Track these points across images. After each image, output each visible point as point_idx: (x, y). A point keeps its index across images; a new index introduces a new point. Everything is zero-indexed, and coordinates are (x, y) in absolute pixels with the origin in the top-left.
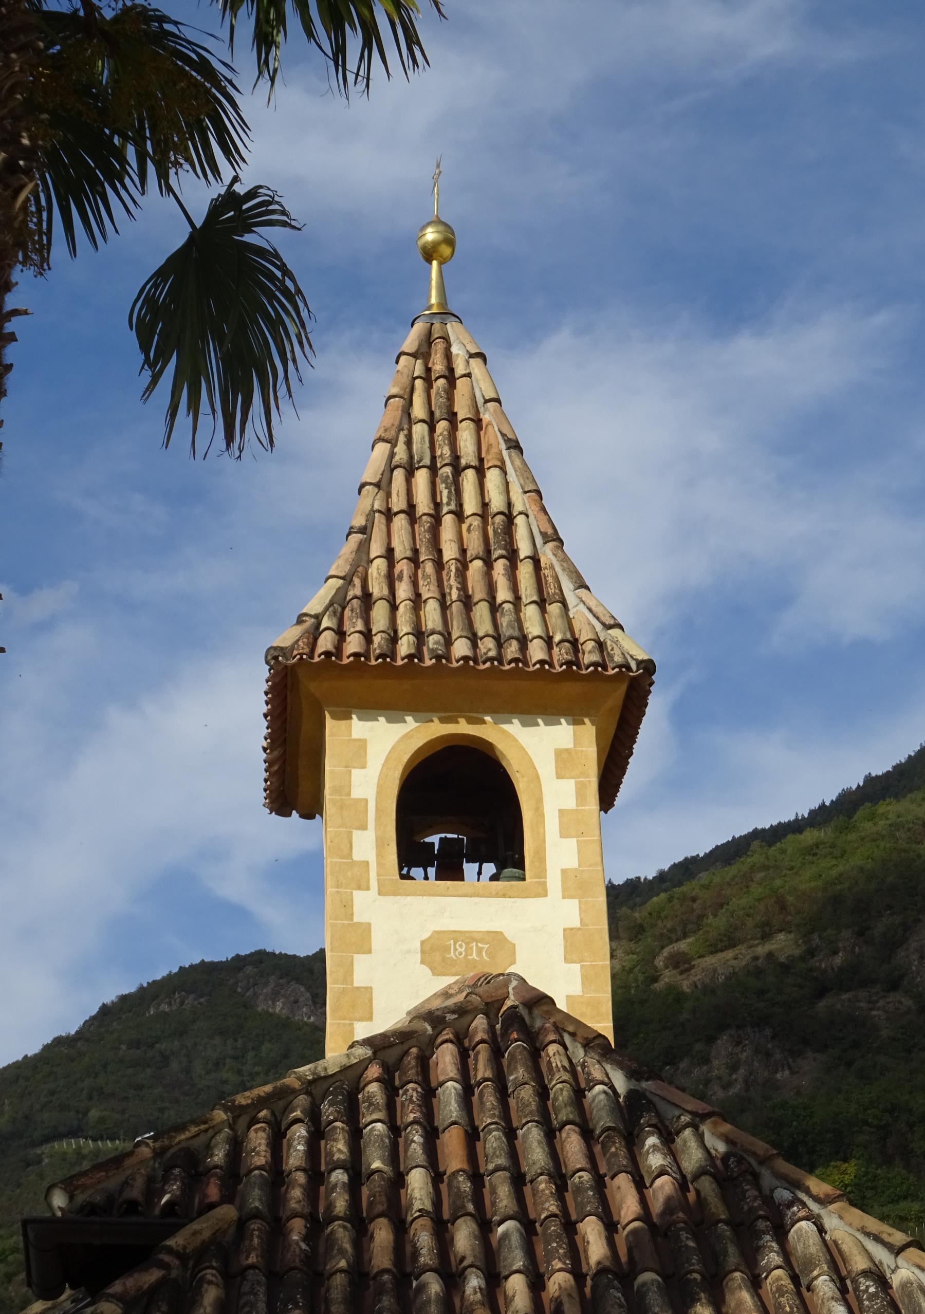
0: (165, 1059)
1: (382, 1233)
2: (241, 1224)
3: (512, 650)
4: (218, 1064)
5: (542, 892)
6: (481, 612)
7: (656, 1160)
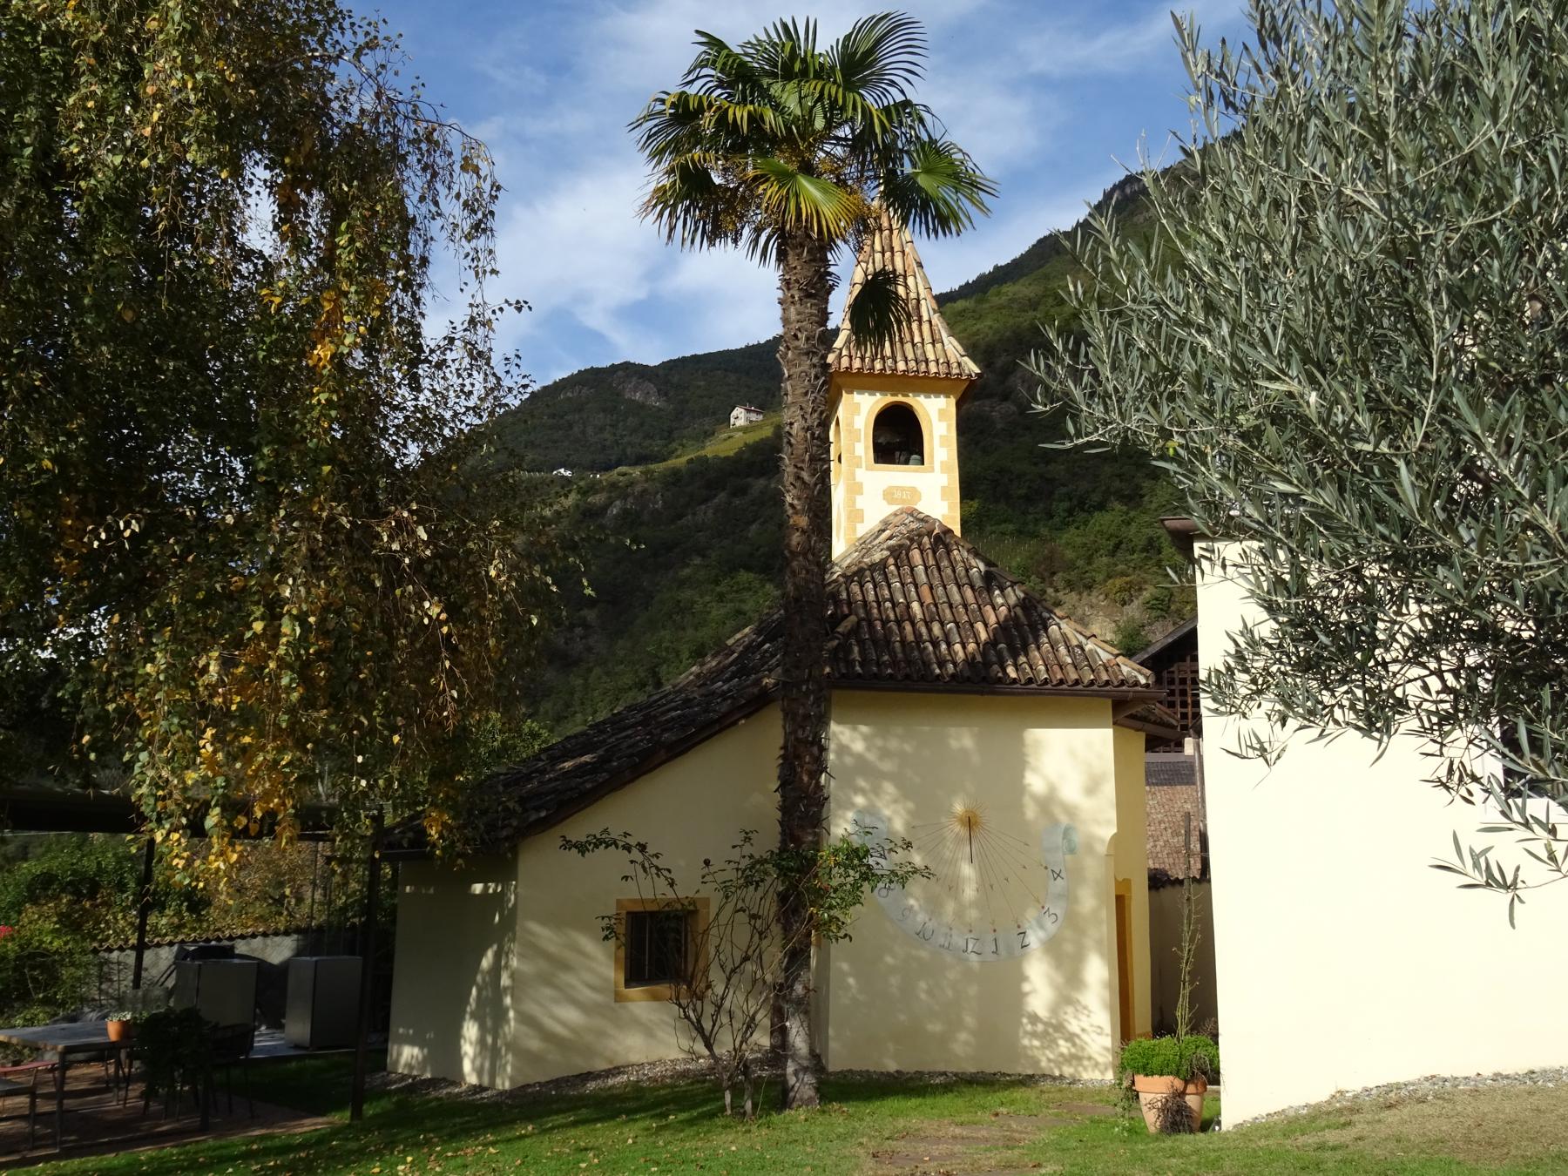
0: (571, 426)
1: (908, 627)
2: (858, 623)
3: (923, 367)
4: (602, 429)
5: (932, 470)
6: (908, 347)
7: (1000, 600)
